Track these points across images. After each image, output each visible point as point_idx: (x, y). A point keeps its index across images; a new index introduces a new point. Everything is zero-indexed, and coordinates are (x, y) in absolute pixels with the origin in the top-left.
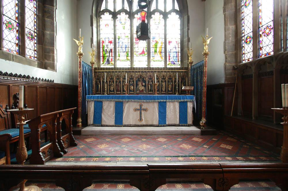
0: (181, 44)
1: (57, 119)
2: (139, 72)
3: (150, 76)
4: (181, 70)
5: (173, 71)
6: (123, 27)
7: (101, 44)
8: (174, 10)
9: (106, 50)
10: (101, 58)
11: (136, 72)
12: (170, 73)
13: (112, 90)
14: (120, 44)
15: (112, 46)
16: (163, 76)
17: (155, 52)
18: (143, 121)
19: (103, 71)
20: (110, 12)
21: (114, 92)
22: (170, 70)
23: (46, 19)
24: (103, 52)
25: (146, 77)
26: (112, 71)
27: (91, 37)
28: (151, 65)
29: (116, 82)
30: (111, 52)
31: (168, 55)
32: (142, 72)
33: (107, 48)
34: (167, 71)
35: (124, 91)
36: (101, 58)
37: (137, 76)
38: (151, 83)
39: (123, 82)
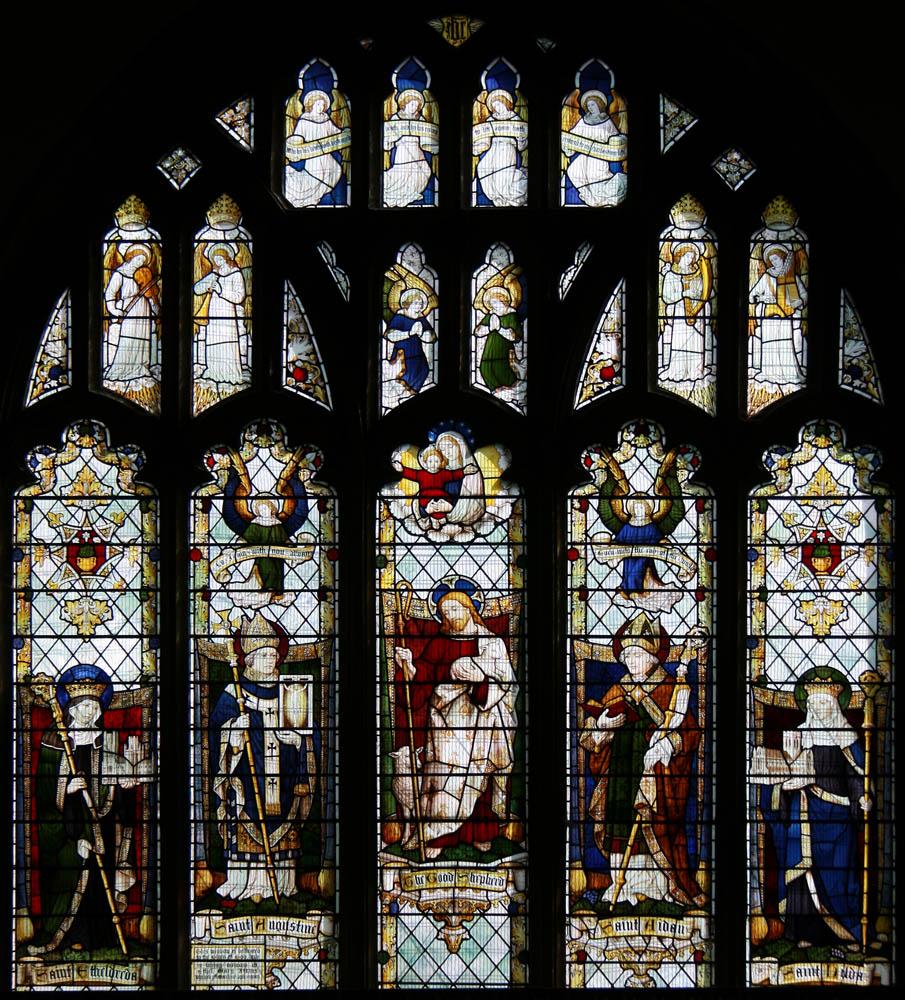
17: (621, 811)
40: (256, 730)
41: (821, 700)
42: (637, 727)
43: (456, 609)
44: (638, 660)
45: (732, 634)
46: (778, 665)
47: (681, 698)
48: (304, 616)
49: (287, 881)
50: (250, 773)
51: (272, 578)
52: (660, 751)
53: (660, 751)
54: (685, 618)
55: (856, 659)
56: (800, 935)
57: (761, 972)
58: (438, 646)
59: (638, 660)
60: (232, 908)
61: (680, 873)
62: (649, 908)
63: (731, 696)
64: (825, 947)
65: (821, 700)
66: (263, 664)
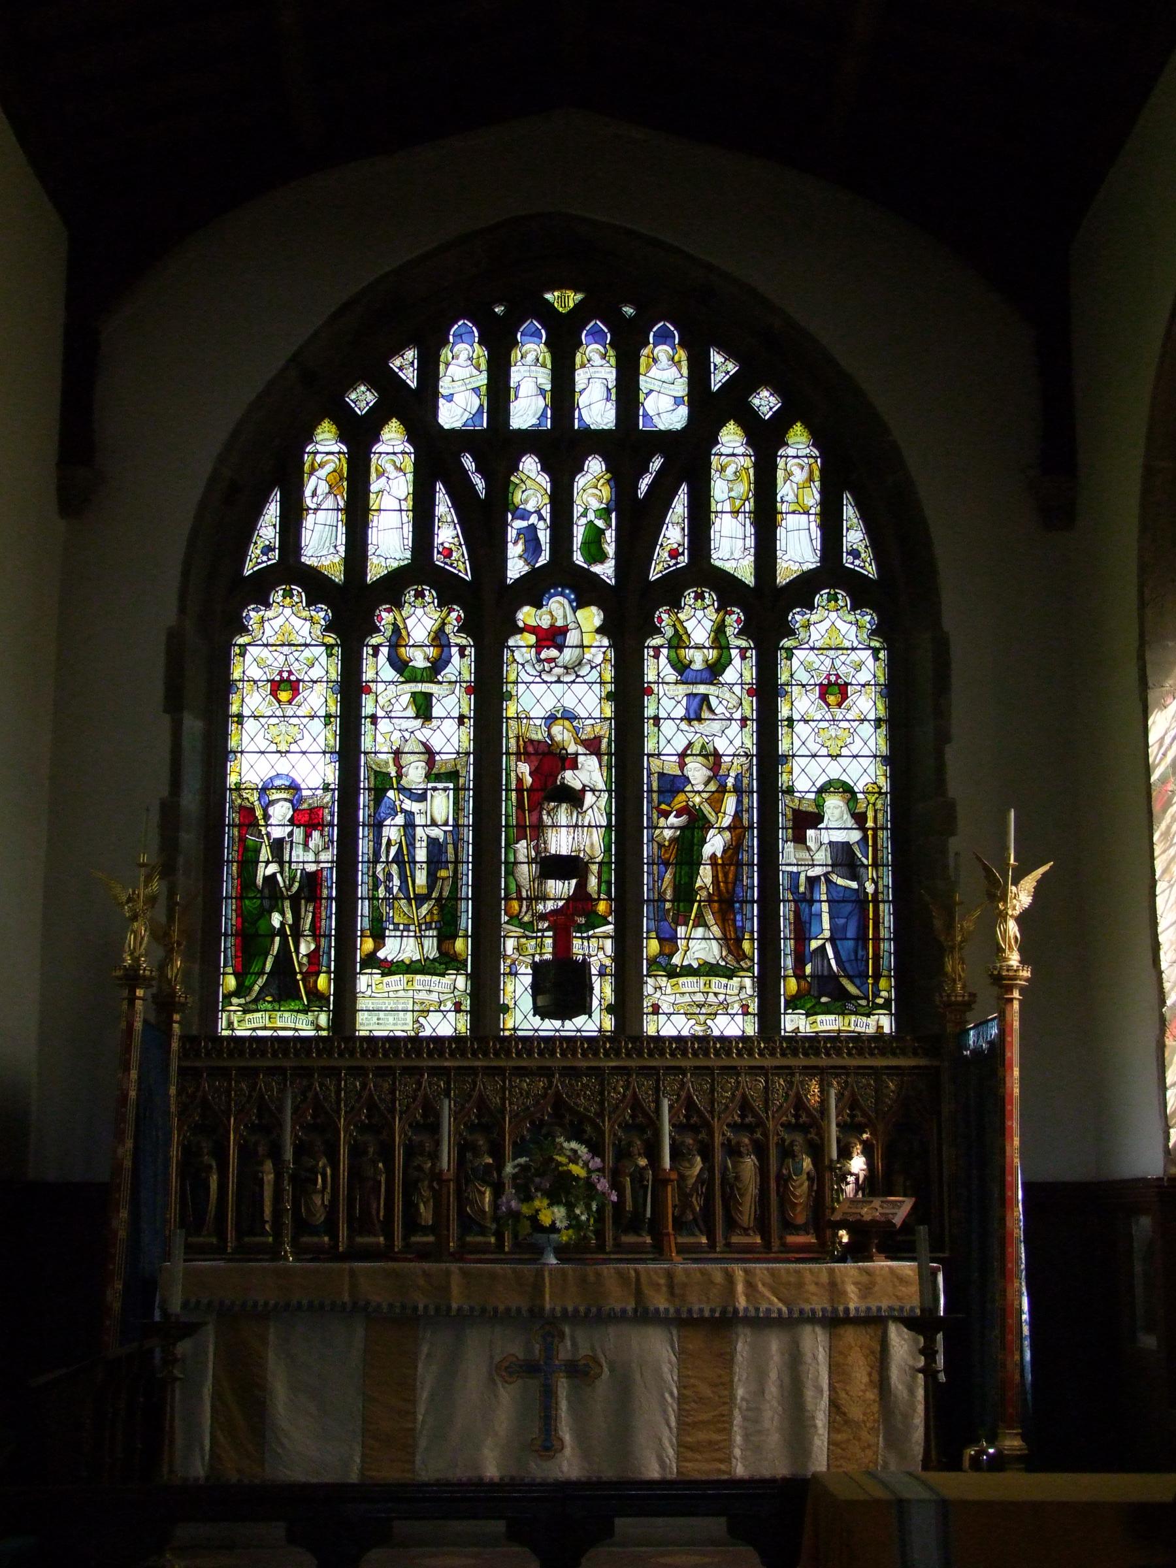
0: (894, 839)
1: (1040, 883)
2: (547, 1072)
3: (745, 1106)
4: (883, 1054)
5: (823, 1061)
6: (420, 699)
7: (231, 834)
8: (831, 573)
9: (270, 880)
10: (227, 945)
11: (521, 1072)
12: (797, 1078)
13: (320, 1217)
14: (392, 832)
15: (313, 855)
16: (797, 1109)
17: (685, 892)
18: (568, 1451)
19: (253, 1063)
20: (315, 586)
21: (334, 1237)
22: (795, 1053)
23: (814, 1241)
24: (240, 898)
25: (600, 1115)
26: (323, 1063)
27: (165, 792)
28: (866, 703)
29: (356, 1151)
30: (308, 901)
31: (785, 929)
32: (572, 1072)
33: (273, 868)
34: (769, 1062)
35: (412, 1225)
36: (227, 945)
37: (530, 1102)
38: (643, 1162)
39: (411, 1151)
40: (409, 826)
41: (834, 806)
42: (697, 824)
43: (561, 733)
44: (697, 772)
45: (769, 758)
46: (803, 778)
48: (450, 738)
49: (431, 947)
50: (404, 861)
51: (423, 708)
52: (715, 844)
53: (715, 844)
54: (735, 741)
55: (865, 772)
56: (826, 992)
57: (794, 1022)
58: (550, 760)
59: (697, 772)
60: (389, 968)
61: (731, 942)
62: (708, 970)
63: (773, 810)
64: (841, 1003)
65: (834, 806)
66: (415, 774)
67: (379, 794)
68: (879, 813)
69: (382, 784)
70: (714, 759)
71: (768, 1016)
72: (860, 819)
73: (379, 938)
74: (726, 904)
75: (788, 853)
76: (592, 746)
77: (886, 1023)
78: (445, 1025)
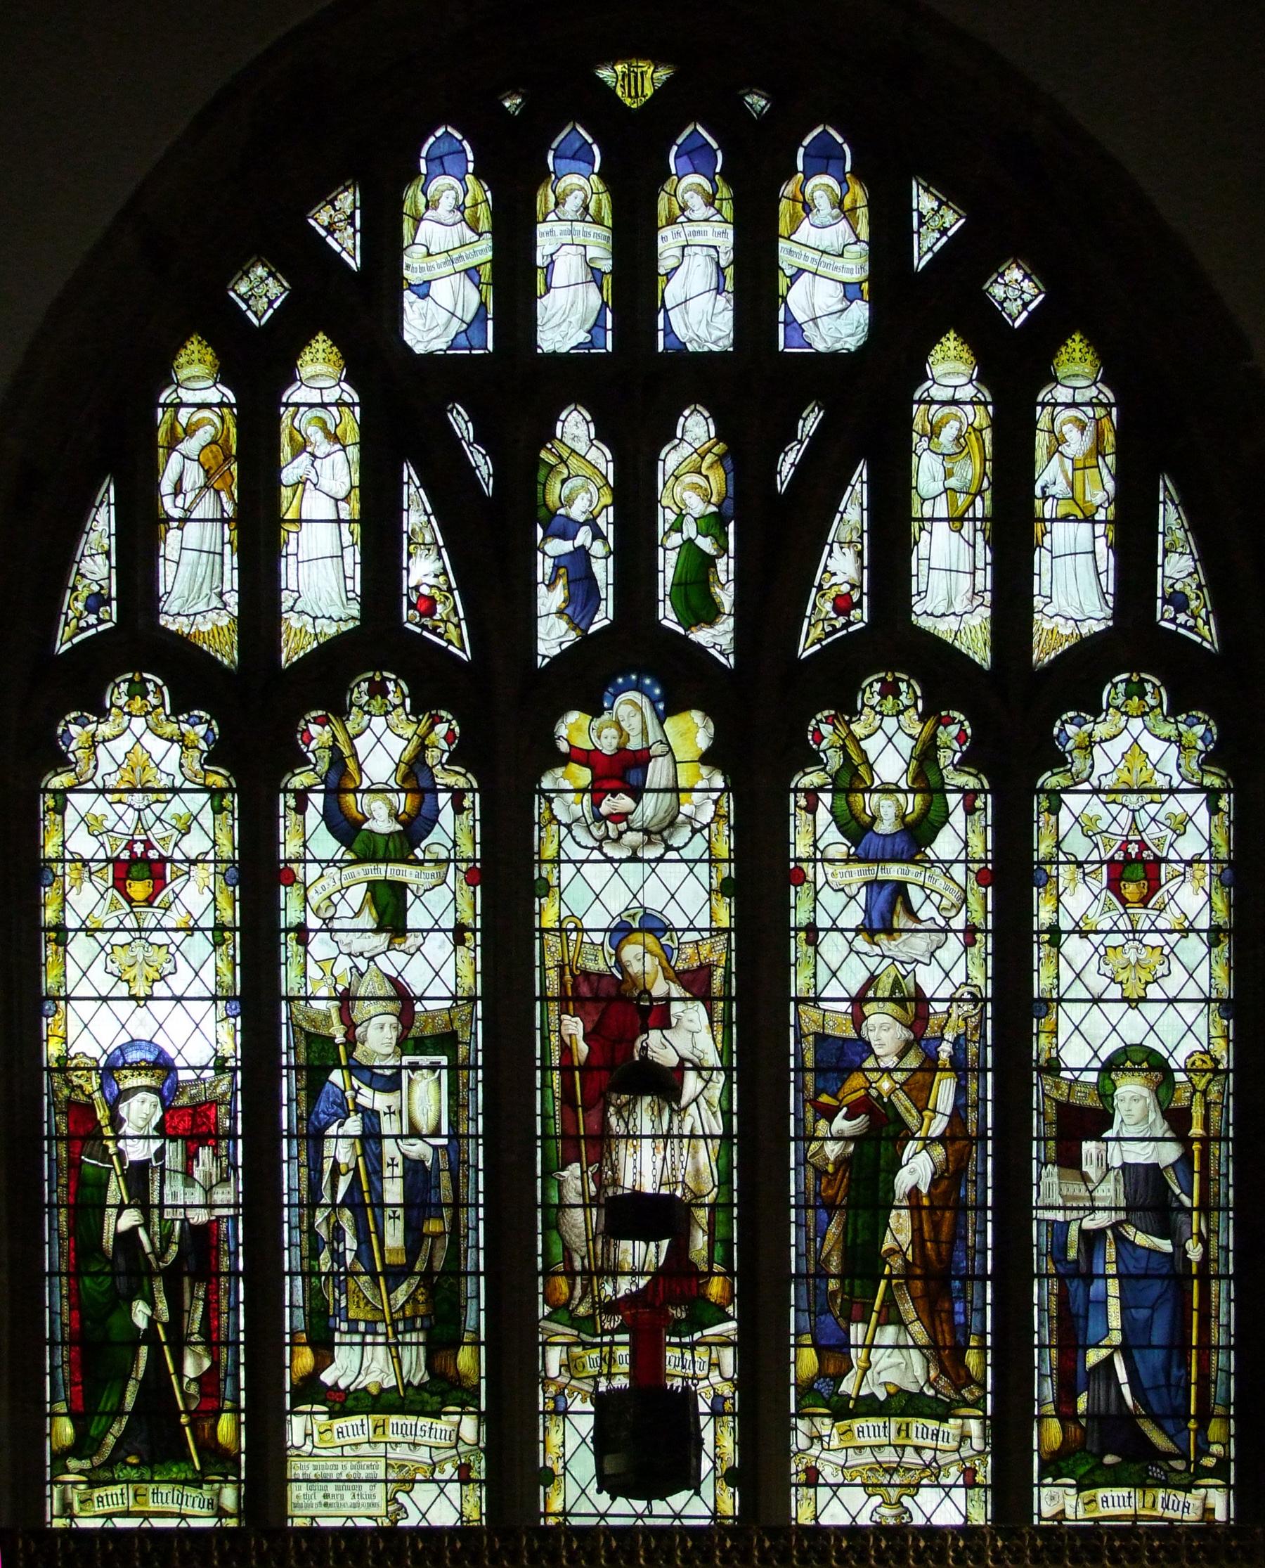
17: (863, 1260)
40: (371, 1137)
41: (1132, 1094)
42: (884, 1133)
44: (885, 1032)
45: (1015, 1003)
46: (1078, 1041)
47: (944, 1092)
48: (439, 969)
49: (414, 1363)
50: (363, 1203)
51: (390, 910)
52: (916, 1169)
53: (916, 1169)
54: (951, 971)
55: (1187, 1032)
56: (1106, 1446)
57: (1055, 1501)
58: (621, 1010)
59: (885, 1032)
60: (343, 1403)
61: (945, 1354)
64: (1141, 1466)
66: (379, 1038)
67: (315, 1077)
68: (1212, 1110)
69: (321, 1056)
70: (914, 1006)
71: (1010, 1491)
72: (1177, 1120)
73: (324, 1350)
74: (936, 1280)
75: (1049, 1184)
76: (696, 983)
77: (1220, 1503)
78: (441, 1507)
